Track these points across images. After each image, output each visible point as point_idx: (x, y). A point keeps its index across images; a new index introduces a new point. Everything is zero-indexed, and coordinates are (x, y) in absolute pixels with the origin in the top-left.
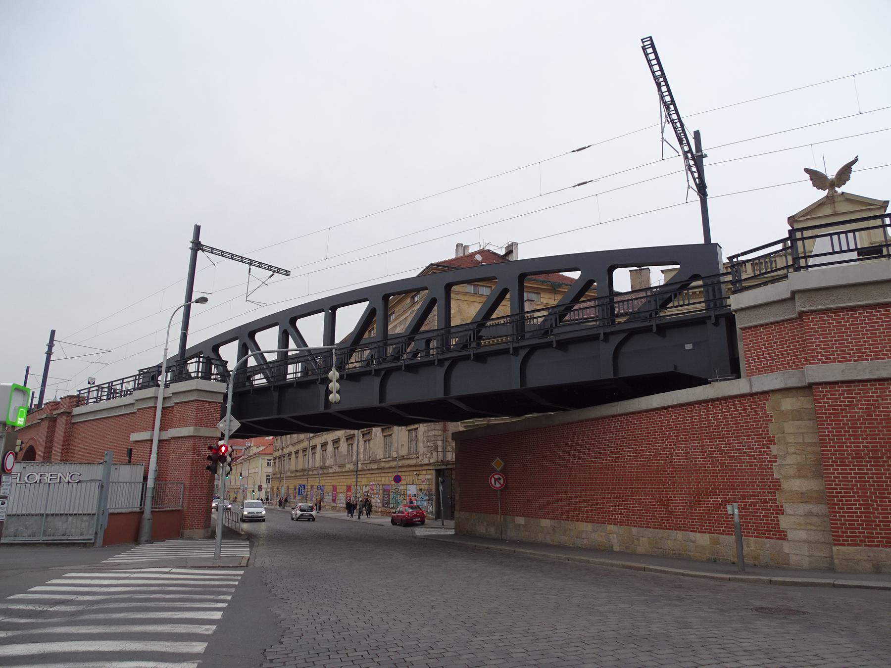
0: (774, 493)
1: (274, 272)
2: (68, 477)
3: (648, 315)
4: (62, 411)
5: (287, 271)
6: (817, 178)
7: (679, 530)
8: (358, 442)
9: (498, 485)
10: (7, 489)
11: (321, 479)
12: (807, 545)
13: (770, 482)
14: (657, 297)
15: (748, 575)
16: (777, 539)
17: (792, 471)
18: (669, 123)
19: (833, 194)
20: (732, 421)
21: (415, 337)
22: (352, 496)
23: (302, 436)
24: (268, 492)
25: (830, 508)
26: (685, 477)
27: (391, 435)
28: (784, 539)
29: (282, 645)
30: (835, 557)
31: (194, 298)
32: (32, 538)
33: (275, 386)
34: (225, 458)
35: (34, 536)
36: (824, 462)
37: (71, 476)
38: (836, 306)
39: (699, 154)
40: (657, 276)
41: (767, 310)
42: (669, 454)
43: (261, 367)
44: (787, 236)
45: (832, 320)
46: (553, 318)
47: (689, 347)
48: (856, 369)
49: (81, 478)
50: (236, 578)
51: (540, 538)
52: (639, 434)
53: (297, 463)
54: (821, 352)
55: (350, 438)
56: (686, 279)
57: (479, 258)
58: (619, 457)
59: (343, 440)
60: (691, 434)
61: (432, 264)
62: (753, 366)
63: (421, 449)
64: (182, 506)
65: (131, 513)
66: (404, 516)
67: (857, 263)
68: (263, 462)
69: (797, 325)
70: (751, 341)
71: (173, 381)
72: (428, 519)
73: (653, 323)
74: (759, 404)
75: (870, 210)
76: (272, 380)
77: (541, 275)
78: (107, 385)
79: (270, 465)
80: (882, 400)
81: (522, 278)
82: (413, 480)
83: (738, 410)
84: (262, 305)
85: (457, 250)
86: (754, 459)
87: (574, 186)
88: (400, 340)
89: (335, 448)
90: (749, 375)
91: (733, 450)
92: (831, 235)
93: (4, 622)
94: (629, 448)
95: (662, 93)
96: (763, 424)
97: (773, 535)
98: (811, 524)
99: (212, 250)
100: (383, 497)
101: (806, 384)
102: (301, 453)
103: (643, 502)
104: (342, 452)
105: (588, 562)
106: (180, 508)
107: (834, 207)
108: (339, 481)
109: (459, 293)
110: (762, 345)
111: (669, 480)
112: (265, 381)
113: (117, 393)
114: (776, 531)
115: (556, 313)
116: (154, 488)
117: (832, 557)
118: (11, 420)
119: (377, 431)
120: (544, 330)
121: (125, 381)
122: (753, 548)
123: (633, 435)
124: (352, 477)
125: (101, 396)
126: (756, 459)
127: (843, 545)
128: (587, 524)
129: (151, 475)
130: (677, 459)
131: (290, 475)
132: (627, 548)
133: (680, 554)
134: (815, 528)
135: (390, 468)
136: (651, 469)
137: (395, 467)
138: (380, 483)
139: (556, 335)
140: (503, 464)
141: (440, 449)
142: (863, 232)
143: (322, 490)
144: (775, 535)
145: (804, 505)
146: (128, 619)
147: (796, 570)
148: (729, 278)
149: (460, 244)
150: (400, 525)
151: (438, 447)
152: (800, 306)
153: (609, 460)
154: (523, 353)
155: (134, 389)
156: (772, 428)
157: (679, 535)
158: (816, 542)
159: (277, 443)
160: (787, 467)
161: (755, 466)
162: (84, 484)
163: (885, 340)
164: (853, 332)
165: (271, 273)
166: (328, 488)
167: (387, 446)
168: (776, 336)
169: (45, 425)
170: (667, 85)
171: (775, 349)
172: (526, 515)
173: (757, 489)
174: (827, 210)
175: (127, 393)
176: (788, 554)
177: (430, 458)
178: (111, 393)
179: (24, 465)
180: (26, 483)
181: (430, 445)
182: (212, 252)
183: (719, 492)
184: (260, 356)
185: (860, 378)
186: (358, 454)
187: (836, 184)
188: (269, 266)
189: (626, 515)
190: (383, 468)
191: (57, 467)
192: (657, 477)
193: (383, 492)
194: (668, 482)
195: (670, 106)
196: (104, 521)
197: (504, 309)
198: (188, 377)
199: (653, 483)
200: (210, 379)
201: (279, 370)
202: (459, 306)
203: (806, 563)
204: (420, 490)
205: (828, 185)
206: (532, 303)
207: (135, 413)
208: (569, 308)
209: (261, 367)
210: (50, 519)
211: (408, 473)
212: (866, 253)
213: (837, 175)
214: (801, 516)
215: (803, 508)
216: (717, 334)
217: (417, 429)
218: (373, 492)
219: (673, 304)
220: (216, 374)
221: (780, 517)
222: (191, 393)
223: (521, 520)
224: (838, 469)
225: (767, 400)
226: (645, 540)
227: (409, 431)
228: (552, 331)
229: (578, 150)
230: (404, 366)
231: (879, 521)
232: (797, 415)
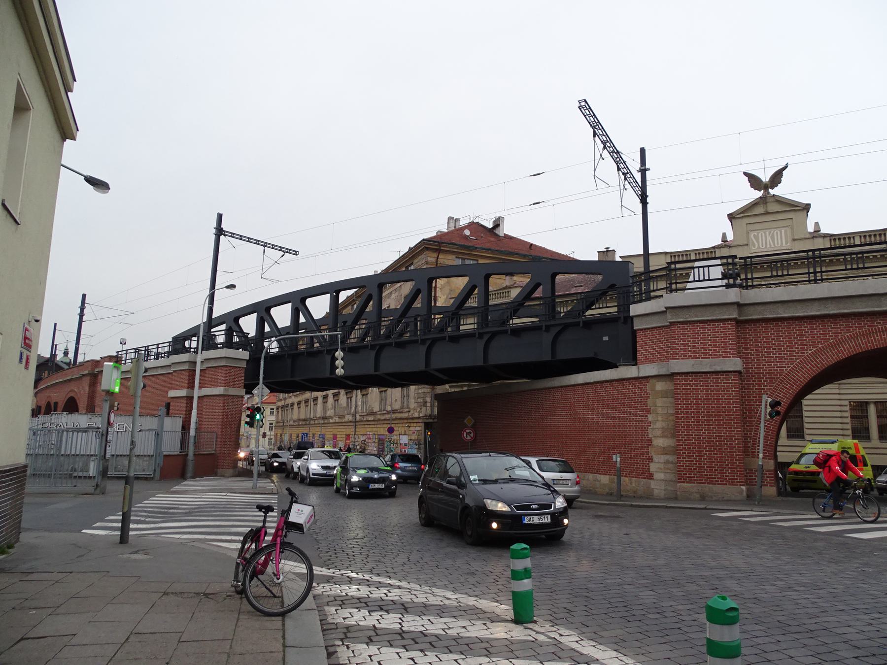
0: (648, 447)
1: (285, 253)
5: (295, 251)
6: (754, 181)
7: (591, 473)
8: (356, 396)
9: (469, 438)
11: (322, 428)
17: (659, 433)
22: (351, 444)
24: (272, 439)
36: (677, 427)
38: (693, 319)
39: (643, 168)
47: (606, 338)
53: (299, 413)
56: (605, 288)
57: (467, 232)
61: (424, 240)
63: (412, 405)
64: (215, 451)
78: (144, 349)
79: (273, 414)
82: (405, 431)
84: (275, 281)
85: (448, 223)
87: (530, 205)
89: (335, 400)
98: (668, 469)
99: (232, 235)
100: (379, 445)
101: (670, 373)
102: (303, 405)
104: (341, 404)
106: (213, 452)
107: (766, 207)
108: (339, 430)
116: (195, 436)
122: (634, 485)
124: (350, 427)
127: (684, 482)
131: (293, 424)
133: (590, 490)
134: (671, 472)
135: (385, 420)
137: (389, 420)
138: (376, 433)
140: (473, 421)
141: (428, 405)
143: (324, 438)
145: (665, 456)
147: (657, 499)
151: (428, 403)
154: (486, 337)
156: (650, 402)
157: (590, 476)
160: (657, 430)
162: (143, 432)
165: (283, 253)
166: (329, 436)
167: (383, 400)
169: (87, 381)
181: (419, 401)
184: (273, 323)
186: (356, 407)
187: (769, 186)
190: (379, 420)
193: (379, 441)
196: (160, 461)
198: (215, 346)
203: (662, 494)
204: (411, 440)
205: (763, 188)
210: (119, 458)
211: (401, 425)
214: (662, 463)
218: (370, 441)
219: (596, 306)
221: (651, 464)
222: (221, 359)
229: (534, 175)
231: (707, 467)
232: (664, 394)
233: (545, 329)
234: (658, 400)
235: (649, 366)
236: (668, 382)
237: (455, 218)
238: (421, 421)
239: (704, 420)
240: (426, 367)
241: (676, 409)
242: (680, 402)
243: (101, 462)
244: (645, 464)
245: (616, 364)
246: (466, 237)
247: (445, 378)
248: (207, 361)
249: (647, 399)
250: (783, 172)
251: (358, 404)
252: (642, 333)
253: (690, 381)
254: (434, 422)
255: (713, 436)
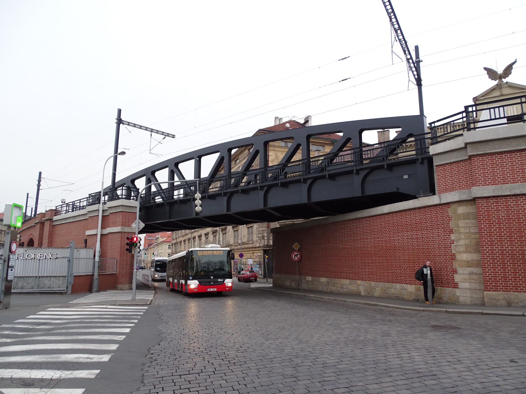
0: (452, 261)
1: (166, 136)
2: (50, 256)
3: (382, 158)
4: (47, 218)
5: (173, 135)
6: (491, 73)
7: (398, 283)
8: (219, 235)
9: (296, 258)
10: (13, 262)
12: (469, 291)
13: (450, 255)
14: (388, 148)
15: (434, 308)
16: (453, 287)
17: (462, 249)
18: (397, 41)
19: (501, 83)
20: (429, 220)
21: (247, 173)
23: (187, 231)
25: (483, 270)
26: (402, 253)
27: (238, 230)
28: (457, 288)
29: (160, 346)
30: (485, 297)
31: (119, 152)
32: (31, 290)
33: (167, 203)
34: (137, 244)
35: (32, 288)
36: (481, 243)
37: (28, 255)
39: (418, 60)
40: (393, 134)
41: (451, 154)
42: (393, 239)
43: (159, 191)
44: (464, 110)
45: (488, 160)
46: (327, 161)
47: (406, 177)
48: (501, 189)
49: (58, 256)
50: (142, 311)
51: (320, 288)
52: (376, 228)
54: (481, 179)
55: (214, 232)
56: (405, 137)
57: (288, 125)
58: (365, 241)
59: (211, 233)
60: (405, 228)
61: (260, 130)
62: (442, 188)
63: (255, 238)
64: (116, 272)
65: (87, 275)
66: (245, 277)
67: (506, 125)
68: (166, 246)
69: (468, 163)
70: (441, 173)
71: (109, 200)
72: (259, 278)
73: (385, 163)
74: (445, 210)
75: (523, 92)
76: (165, 199)
77: (324, 135)
78: (71, 203)
80: (516, 207)
81: (309, 137)
82: (251, 256)
83: (433, 214)
85: (275, 121)
86: (441, 242)
87: (340, 82)
88: (237, 175)
89: (206, 238)
90: (440, 193)
91: (429, 237)
92: (490, 109)
93: (10, 334)
94: (371, 237)
95: (393, 23)
96: (446, 222)
97: (451, 285)
98: (472, 279)
99: (129, 124)
101: (472, 198)
102: (187, 241)
103: (378, 267)
105: (345, 301)
109: (274, 146)
110: (448, 175)
111: (393, 254)
112: (161, 200)
113: (77, 208)
114: (452, 283)
115: (328, 158)
116: (99, 262)
117: (483, 298)
118: (13, 224)
119: (230, 228)
120: (322, 168)
121: (81, 201)
123: (373, 229)
125: (69, 209)
126: (442, 242)
127: (490, 291)
128: (347, 280)
129: (97, 254)
130: (397, 243)
132: (369, 293)
134: (475, 281)
135: (237, 249)
136: (382, 248)
137: (240, 249)
139: (328, 171)
141: (266, 238)
142: (515, 106)
144: (452, 285)
145: (469, 268)
146: (78, 332)
147: (463, 305)
148: (429, 136)
149: (277, 117)
150: (243, 282)
152: (470, 152)
153: (359, 243)
154: (309, 182)
155: (87, 205)
156: (452, 224)
157: (398, 286)
158: (475, 289)
159: (173, 236)
160: (460, 246)
161: (442, 246)
162: (59, 259)
163: (519, 171)
164: (500, 167)
168: (455, 170)
169: (38, 226)
170: (396, 17)
171: (455, 178)
172: (312, 275)
173: (442, 259)
174: (497, 93)
175: (83, 207)
176: (459, 297)
177: (260, 243)
178: (75, 208)
179: (26, 249)
180: (27, 259)
182: (129, 125)
183: (421, 261)
184: (158, 185)
185: (503, 194)
186: (219, 241)
188: (163, 132)
189: (368, 274)
191: (44, 250)
192: (386, 253)
194: (392, 256)
195: (398, 31)
196: (71, 280)
197: (298, 156)
199: (384, 256)
200: (130, 199)
201: (169, 193)
202: (276, 154)
203: (468, 301)
204: (254, 262)
205: (498, 77)
206: (319, 152)
207: (88, 219)
208: (335, 155)
209: (159, 191)
210: (41, 279)
211: (248, 252)
212: (512, 119)
213: (504, 71)
214: (466, 274)
215: (468, 270)
216: (422, 169)
217: (252, 226)
220: (133, 196)
221: (455, 275)
223: (309, 278)
224: (489, 248)
225: (449, 208)
226: (379, 289)
227: (248, 228)
228: (326, 169)
230: (259, 187)
232: (466, 216)
233: (356, 172)
234: (460, 222)
235: (450, 194)
236: (469, 207)
237: (279, 118)
238: (261, 249)
239: (507, 236)
240: (264, 207)
241: (479, 228)
242: (483, 222)
243: (4, 283)
244: (449, 275)
245: (415, 196)
246: (287, 129)
247: (277, 214)
248: (110, 209)
249: (449, 222)
250: (513, 66)
251: (220, 239)
252: (441, 168)
253: (491, 204)
254: (270, 249)
255: (516, 250)
